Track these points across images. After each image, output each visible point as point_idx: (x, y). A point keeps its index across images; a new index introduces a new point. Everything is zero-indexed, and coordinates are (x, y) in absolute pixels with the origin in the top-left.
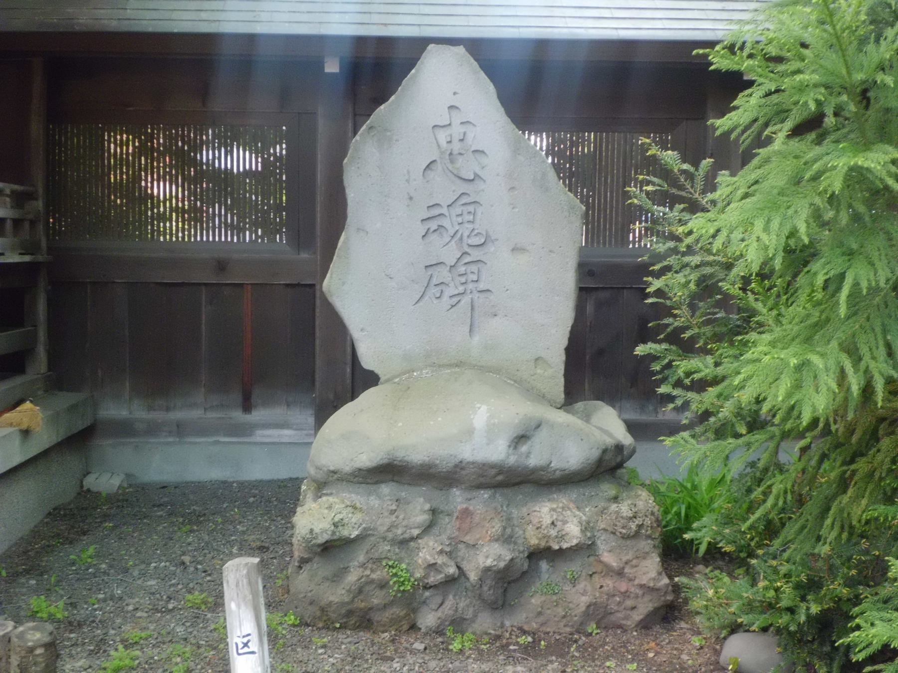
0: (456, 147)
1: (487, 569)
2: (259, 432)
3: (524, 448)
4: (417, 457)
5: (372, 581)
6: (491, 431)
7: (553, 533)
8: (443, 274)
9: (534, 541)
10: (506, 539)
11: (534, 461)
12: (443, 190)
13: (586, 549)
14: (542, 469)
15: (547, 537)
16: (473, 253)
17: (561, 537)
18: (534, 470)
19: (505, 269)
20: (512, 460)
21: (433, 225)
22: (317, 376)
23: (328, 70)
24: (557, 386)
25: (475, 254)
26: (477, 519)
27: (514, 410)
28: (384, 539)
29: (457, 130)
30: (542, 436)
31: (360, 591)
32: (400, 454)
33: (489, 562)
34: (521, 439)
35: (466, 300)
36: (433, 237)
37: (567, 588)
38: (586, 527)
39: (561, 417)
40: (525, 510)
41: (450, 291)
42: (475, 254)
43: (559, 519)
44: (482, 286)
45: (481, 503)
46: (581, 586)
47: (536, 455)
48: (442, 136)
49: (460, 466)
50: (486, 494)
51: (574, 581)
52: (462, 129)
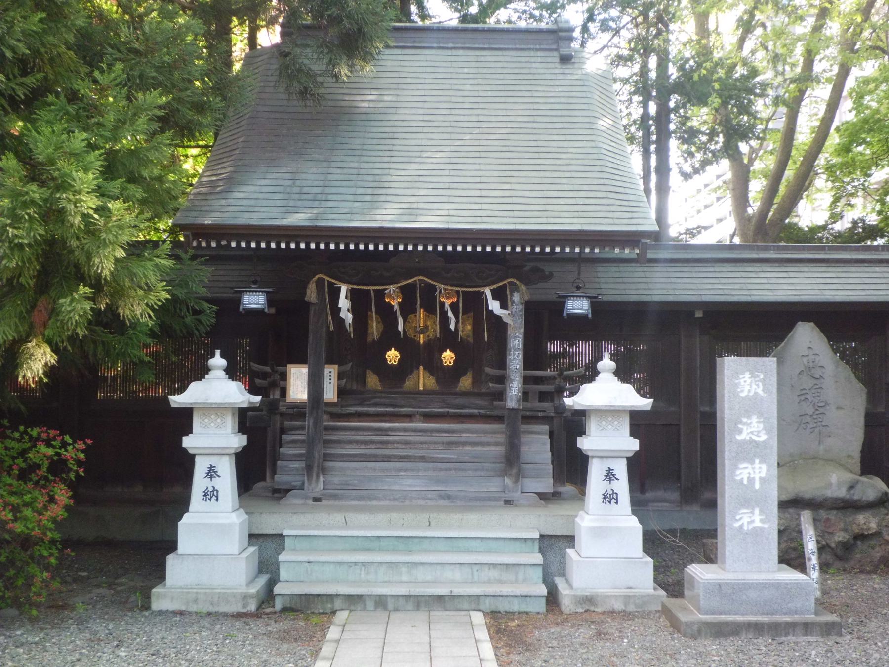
0: (811, 364)
1: (840, 542)
2: (650, 504)
3: (852, 492)
4: (808, 496)
5: (791, 548)
6: (839, 485)
7: (865, 527)
8: (808, 419)
9: (857, 531)
10: (845, 530)
11: (856, 497)
12: (808, 383)
13: (878, 534)
14: (860, 500)
15: (862, 529)
16: (820, 408)
17: (869, 529)
18: (856, 501)
19: (833, 416)
20: (848, 496)
21: (802, 398)
22: (682, 473)
23: (697, 315)
24: (858, 468)
25: (821, 410)
26: (833, 522)
27: (848, 477)
28: (794, 530)
29: (812, 357)
30: (859, 486)
31: (787, 552)
32: (801, 494)
33: (840, 539)
34: (851, 487)
35: (817, 430)
36: (802, 403)
37: (870, 550)
38: (879, 525)
39: (863, 479)
40: (851, 519)
41: (809, 426)
42: (821, 410)
43: (868, 522)
44: (824, 424)
45: (833, 515)
46: (877, 549)
47: (857, 495)
48: (805, 360)
49: (826, 499)
50: (835, 512)
51: (873, 548)
52: (813, 357)
